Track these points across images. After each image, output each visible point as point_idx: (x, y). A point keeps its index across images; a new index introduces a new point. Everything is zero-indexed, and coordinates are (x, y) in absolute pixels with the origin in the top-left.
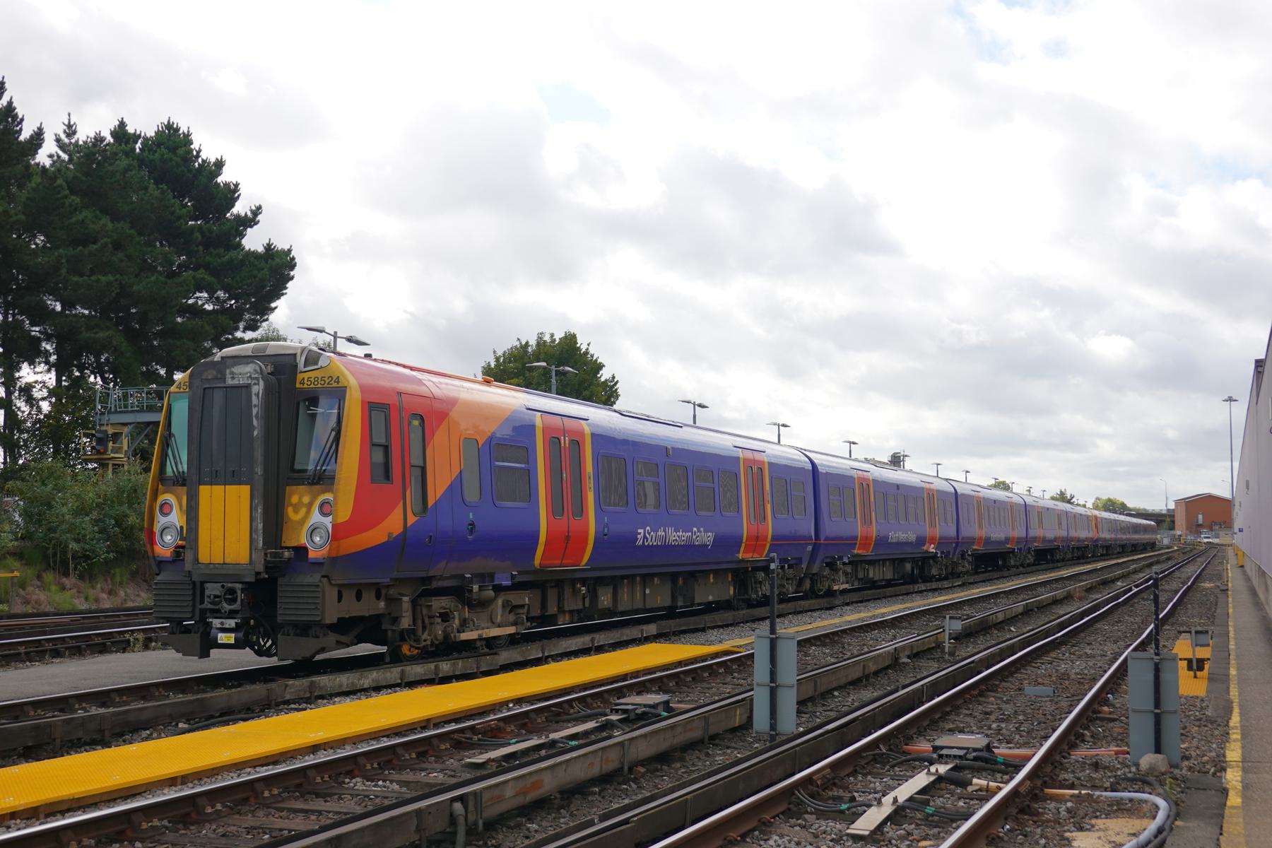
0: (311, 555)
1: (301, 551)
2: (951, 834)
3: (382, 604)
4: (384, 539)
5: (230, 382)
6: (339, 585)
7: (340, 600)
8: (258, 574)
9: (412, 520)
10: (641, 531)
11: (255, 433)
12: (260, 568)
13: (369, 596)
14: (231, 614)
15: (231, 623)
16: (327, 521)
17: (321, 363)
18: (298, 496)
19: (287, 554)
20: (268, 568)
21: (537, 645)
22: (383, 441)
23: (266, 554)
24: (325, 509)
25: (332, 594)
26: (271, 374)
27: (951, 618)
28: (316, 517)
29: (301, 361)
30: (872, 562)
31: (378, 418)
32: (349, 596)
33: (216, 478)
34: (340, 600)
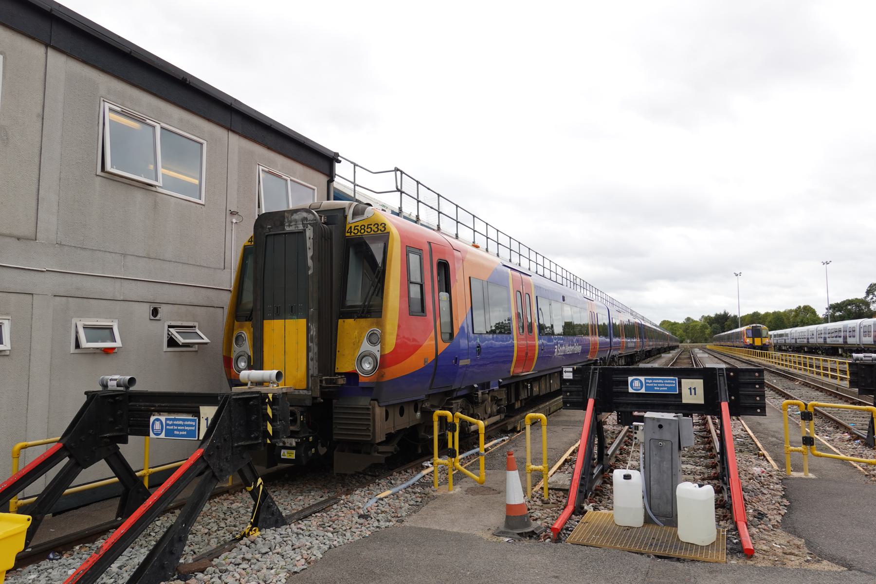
0: (361, 380)
1: (352, 377)
2: (541, 441)
3: (419, 414)
4: (421, 365)
5: (287, 229)
6: (386, 406)
7: (386, 419)
8: (314, 398)
11: (310, 272)
12: (317, 393)
13: (409, 410)
14: (293, 435)
15: (293, 442)
16: (376, 350)
17: (365, 216)
18: (349, 328)
19: (342, 381)
20: (323, 394)
21: (245, 293)
22: (419, 280)
23: (321, 381)
24: (373, 339)
25: (379, 412)
26: (325, 223)
27: (257, 363)
28: (366, 346)
30: (536, 379)
31: (414, 259)
32: (395, 414)
33: (278, 314)
34: (386, 419)
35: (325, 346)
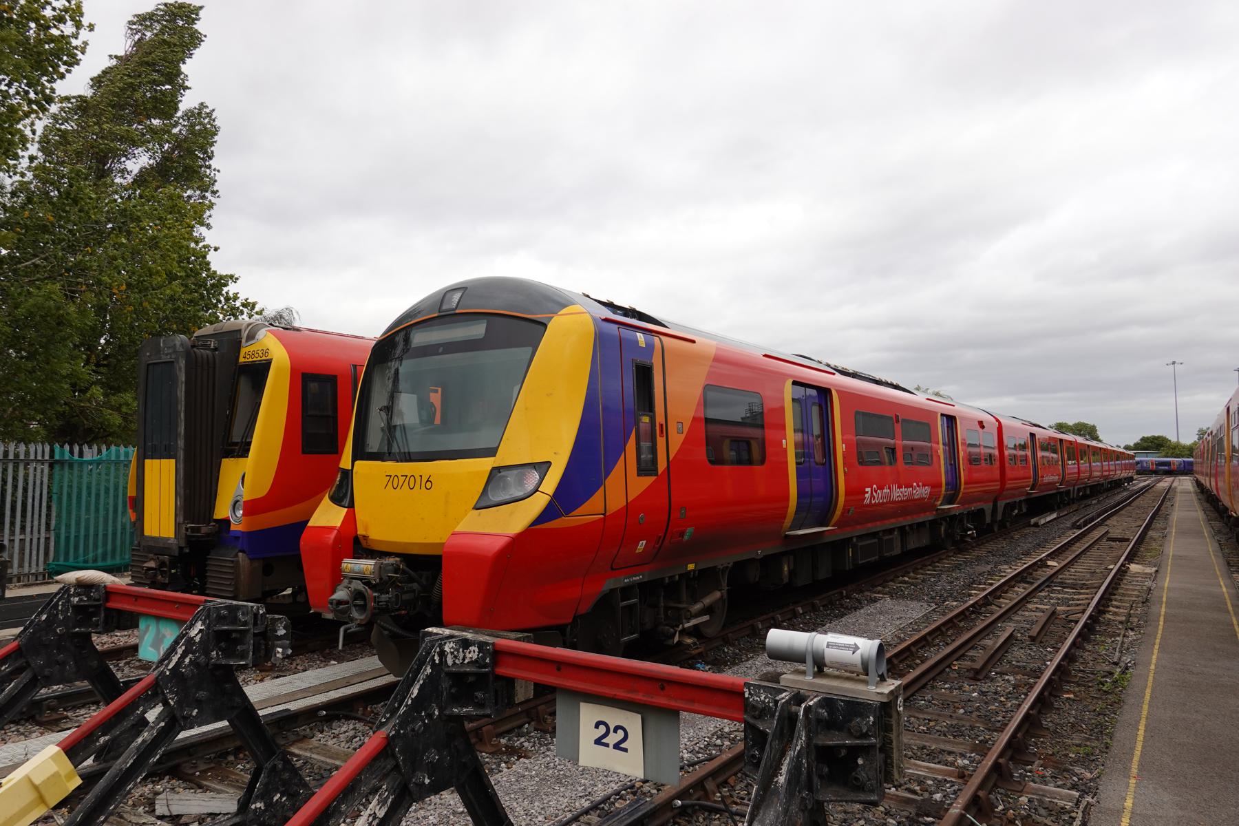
9: (641, 484)
10: (868, 489)
29: (244, 335)
35: (197, 491)
